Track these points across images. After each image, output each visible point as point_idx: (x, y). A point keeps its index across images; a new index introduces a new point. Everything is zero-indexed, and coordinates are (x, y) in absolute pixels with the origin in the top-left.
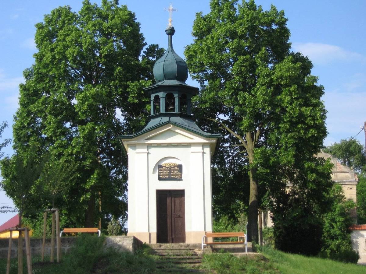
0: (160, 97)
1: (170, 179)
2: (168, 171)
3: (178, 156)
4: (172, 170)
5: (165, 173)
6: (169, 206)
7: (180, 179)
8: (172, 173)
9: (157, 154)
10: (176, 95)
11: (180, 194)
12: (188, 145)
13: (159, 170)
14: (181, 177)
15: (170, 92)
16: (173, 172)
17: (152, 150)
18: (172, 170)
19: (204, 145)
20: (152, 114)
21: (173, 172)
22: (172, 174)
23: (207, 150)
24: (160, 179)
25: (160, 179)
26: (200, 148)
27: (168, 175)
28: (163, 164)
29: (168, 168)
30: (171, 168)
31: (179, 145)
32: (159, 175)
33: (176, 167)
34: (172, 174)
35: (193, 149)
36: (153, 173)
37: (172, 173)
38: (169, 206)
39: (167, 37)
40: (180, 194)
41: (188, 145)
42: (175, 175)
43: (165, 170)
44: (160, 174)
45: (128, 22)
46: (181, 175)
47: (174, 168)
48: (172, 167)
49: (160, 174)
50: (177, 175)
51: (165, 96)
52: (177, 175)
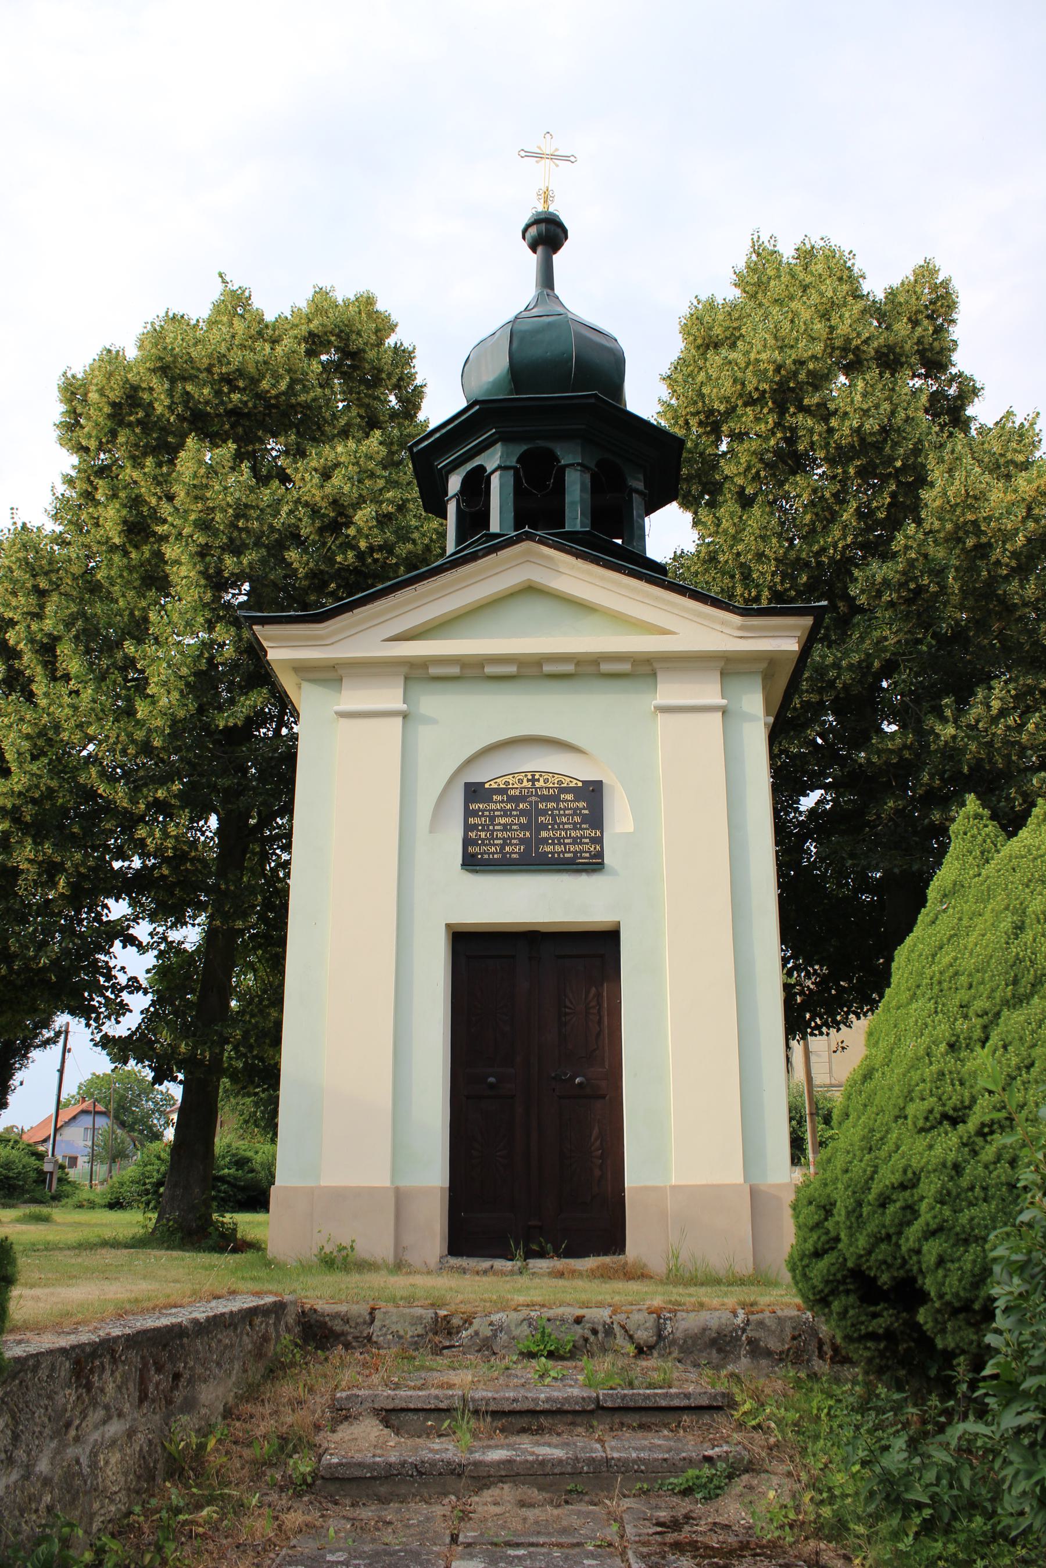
0: (489, 470)
1: (533, 861)
2: (523, 820)
3: (591, 737)
4: (544, 813)
5: (505, 827)
6: (532, 1026)
7: (594, 864)
8: (545, 827)
9: (463, 726)
10: (568, 455)
11: (595, 951)
12: (644, 669)
13: (468, 813)
14: (600, 855)
15: (541, 443)
16: (533, 823)
17: (434, 703)
18: (544, 813)
19: (729, 667)
20: (451, 548)
21: (533, 823)
22: (544, 834)
23: (754, 710)
24: (472, 862)
25: (472, 862)
26: (708, 692)
27: (522, 841)
28: (485, 774)
29: (522, 798)
30: (534, 803)
31: (591, 669)
32: (467, 842)
33: (570, 797)
34: (544, 834)
35: (670, 691)
36: (431, 832)
37: (545, 827)
38: (532, 1026)
39: (531, 260)
40: (595, 951)
41: (644, 669)
42: (560, 841)
43: (506, 813)
44: (472, 835)
45: (894, 1239)
46: (599, 841)
47: (555, 798)
48: (545, 798)
49: (472, 835)
50: (575, 841)
51: (513, 462)
52: (575, 841)
